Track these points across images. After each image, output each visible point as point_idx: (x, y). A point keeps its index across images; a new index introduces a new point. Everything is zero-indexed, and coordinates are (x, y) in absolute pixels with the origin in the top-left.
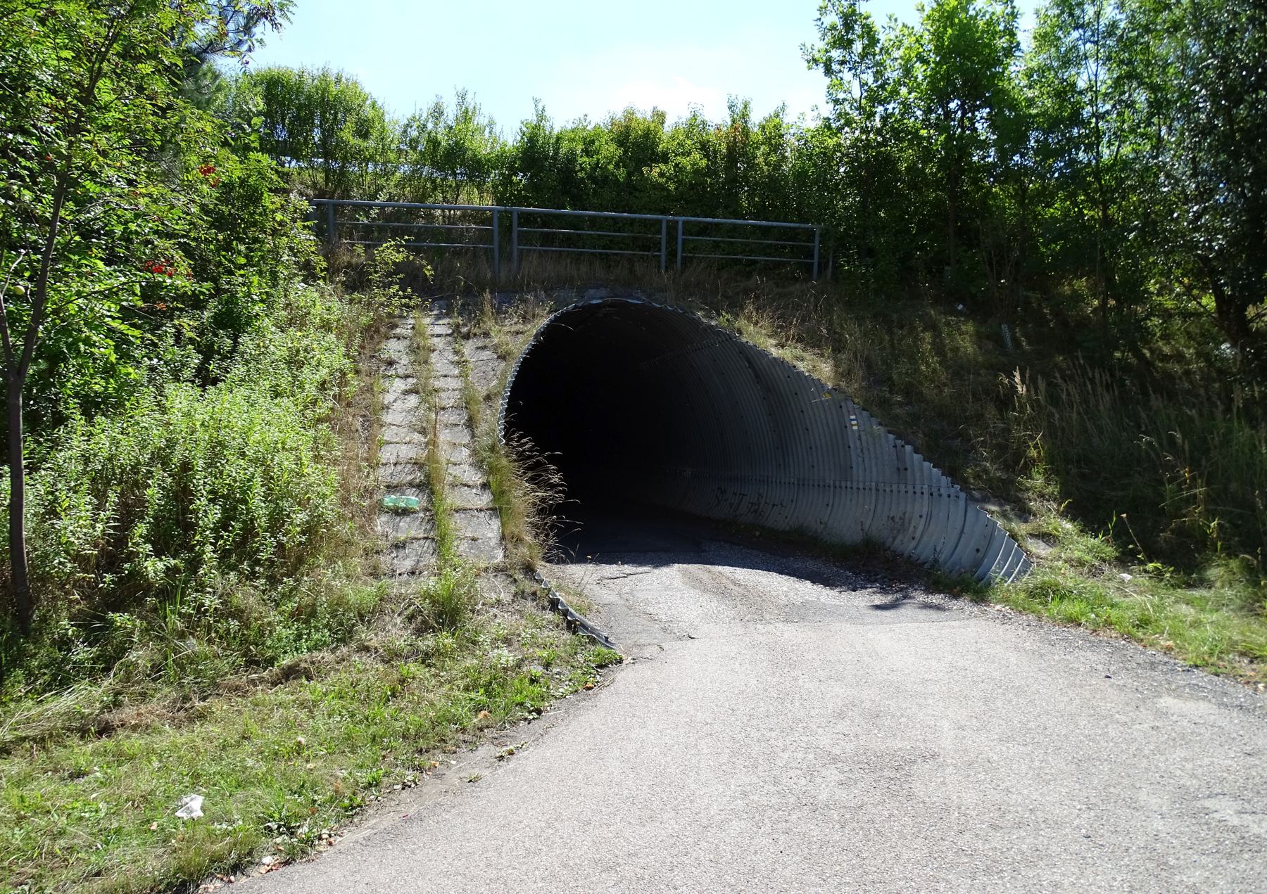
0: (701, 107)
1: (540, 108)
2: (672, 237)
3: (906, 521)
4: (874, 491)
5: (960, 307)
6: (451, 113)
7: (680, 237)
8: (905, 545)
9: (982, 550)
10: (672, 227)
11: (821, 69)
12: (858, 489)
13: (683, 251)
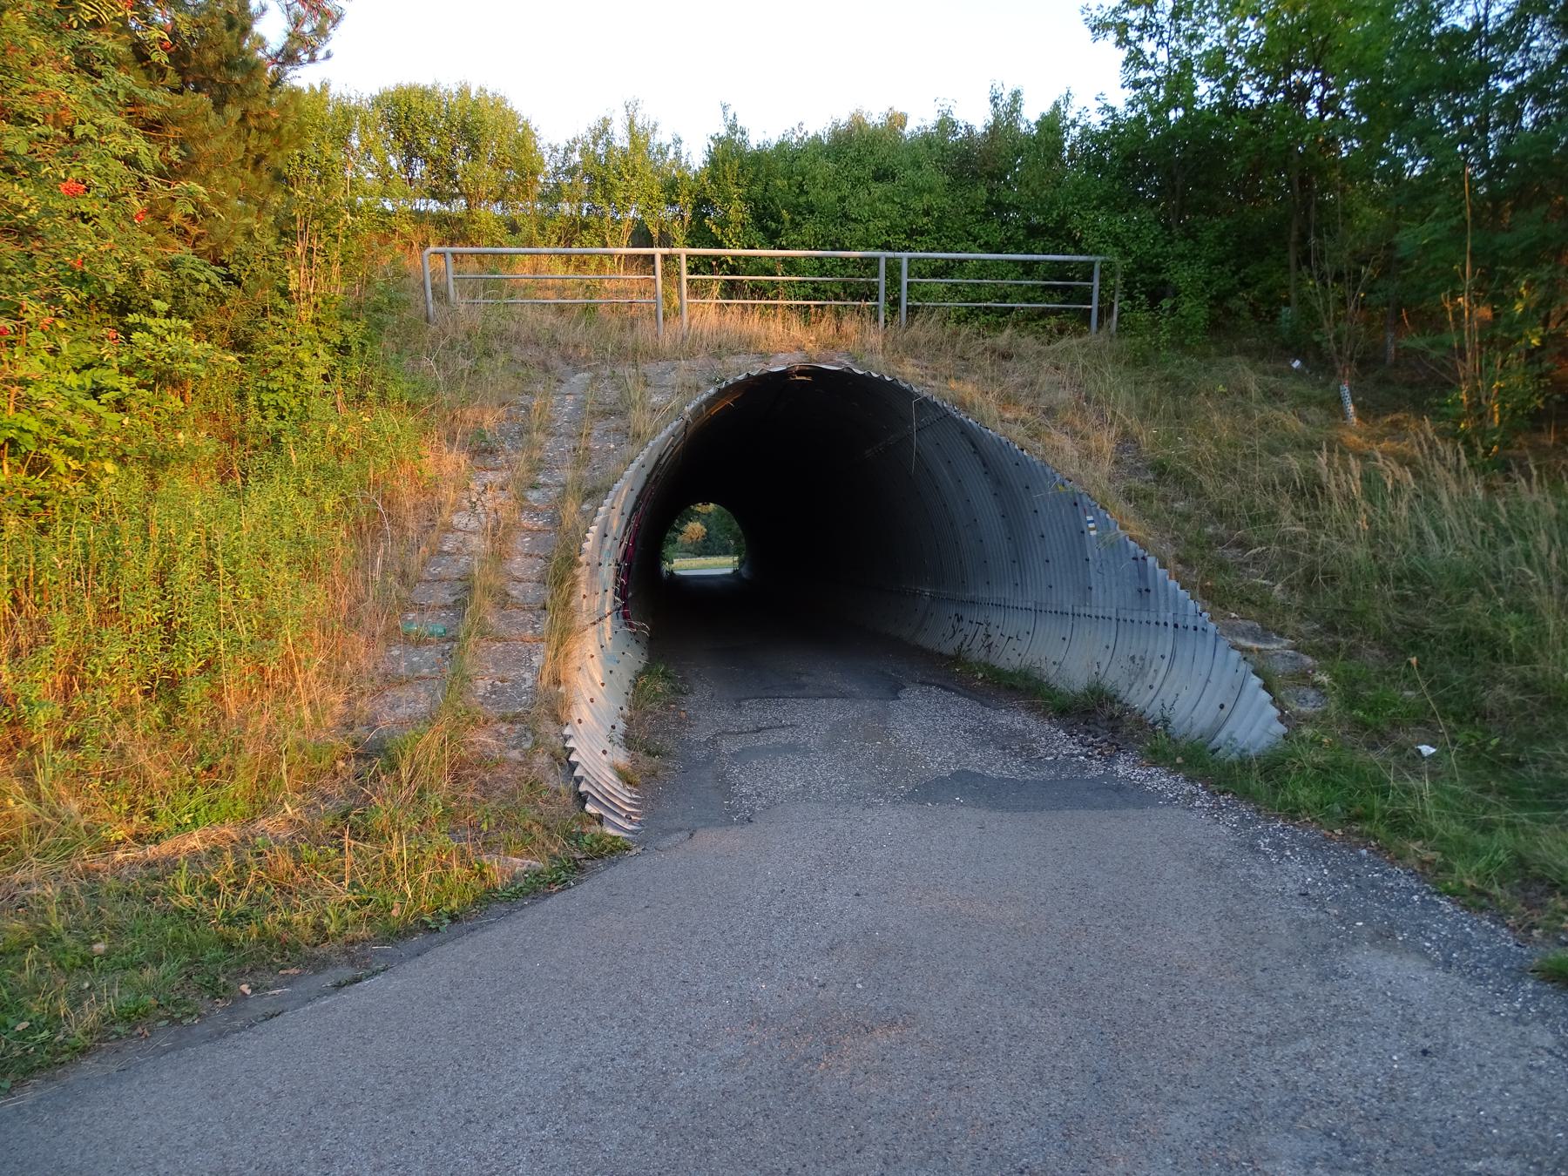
0: (953, 104)
1: (731, 117)
2: (894, 280)
3: (1147, 663)
4: (1114, 620)
5: (1296, 364)
6: (621, 139)
7: (905, 280)
8: (1140, 699)
9: (1228, 706)
10: (893, 269)
11: (1112, 36)
12: (1157, 623)
13: (909, 298)
